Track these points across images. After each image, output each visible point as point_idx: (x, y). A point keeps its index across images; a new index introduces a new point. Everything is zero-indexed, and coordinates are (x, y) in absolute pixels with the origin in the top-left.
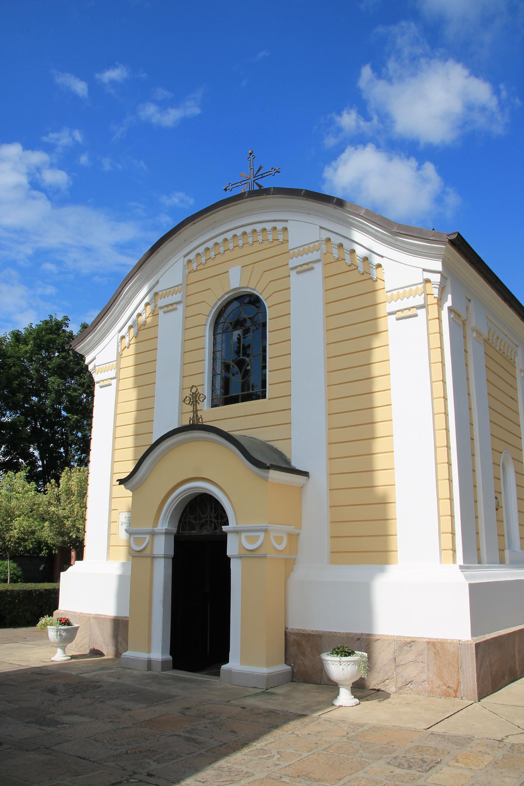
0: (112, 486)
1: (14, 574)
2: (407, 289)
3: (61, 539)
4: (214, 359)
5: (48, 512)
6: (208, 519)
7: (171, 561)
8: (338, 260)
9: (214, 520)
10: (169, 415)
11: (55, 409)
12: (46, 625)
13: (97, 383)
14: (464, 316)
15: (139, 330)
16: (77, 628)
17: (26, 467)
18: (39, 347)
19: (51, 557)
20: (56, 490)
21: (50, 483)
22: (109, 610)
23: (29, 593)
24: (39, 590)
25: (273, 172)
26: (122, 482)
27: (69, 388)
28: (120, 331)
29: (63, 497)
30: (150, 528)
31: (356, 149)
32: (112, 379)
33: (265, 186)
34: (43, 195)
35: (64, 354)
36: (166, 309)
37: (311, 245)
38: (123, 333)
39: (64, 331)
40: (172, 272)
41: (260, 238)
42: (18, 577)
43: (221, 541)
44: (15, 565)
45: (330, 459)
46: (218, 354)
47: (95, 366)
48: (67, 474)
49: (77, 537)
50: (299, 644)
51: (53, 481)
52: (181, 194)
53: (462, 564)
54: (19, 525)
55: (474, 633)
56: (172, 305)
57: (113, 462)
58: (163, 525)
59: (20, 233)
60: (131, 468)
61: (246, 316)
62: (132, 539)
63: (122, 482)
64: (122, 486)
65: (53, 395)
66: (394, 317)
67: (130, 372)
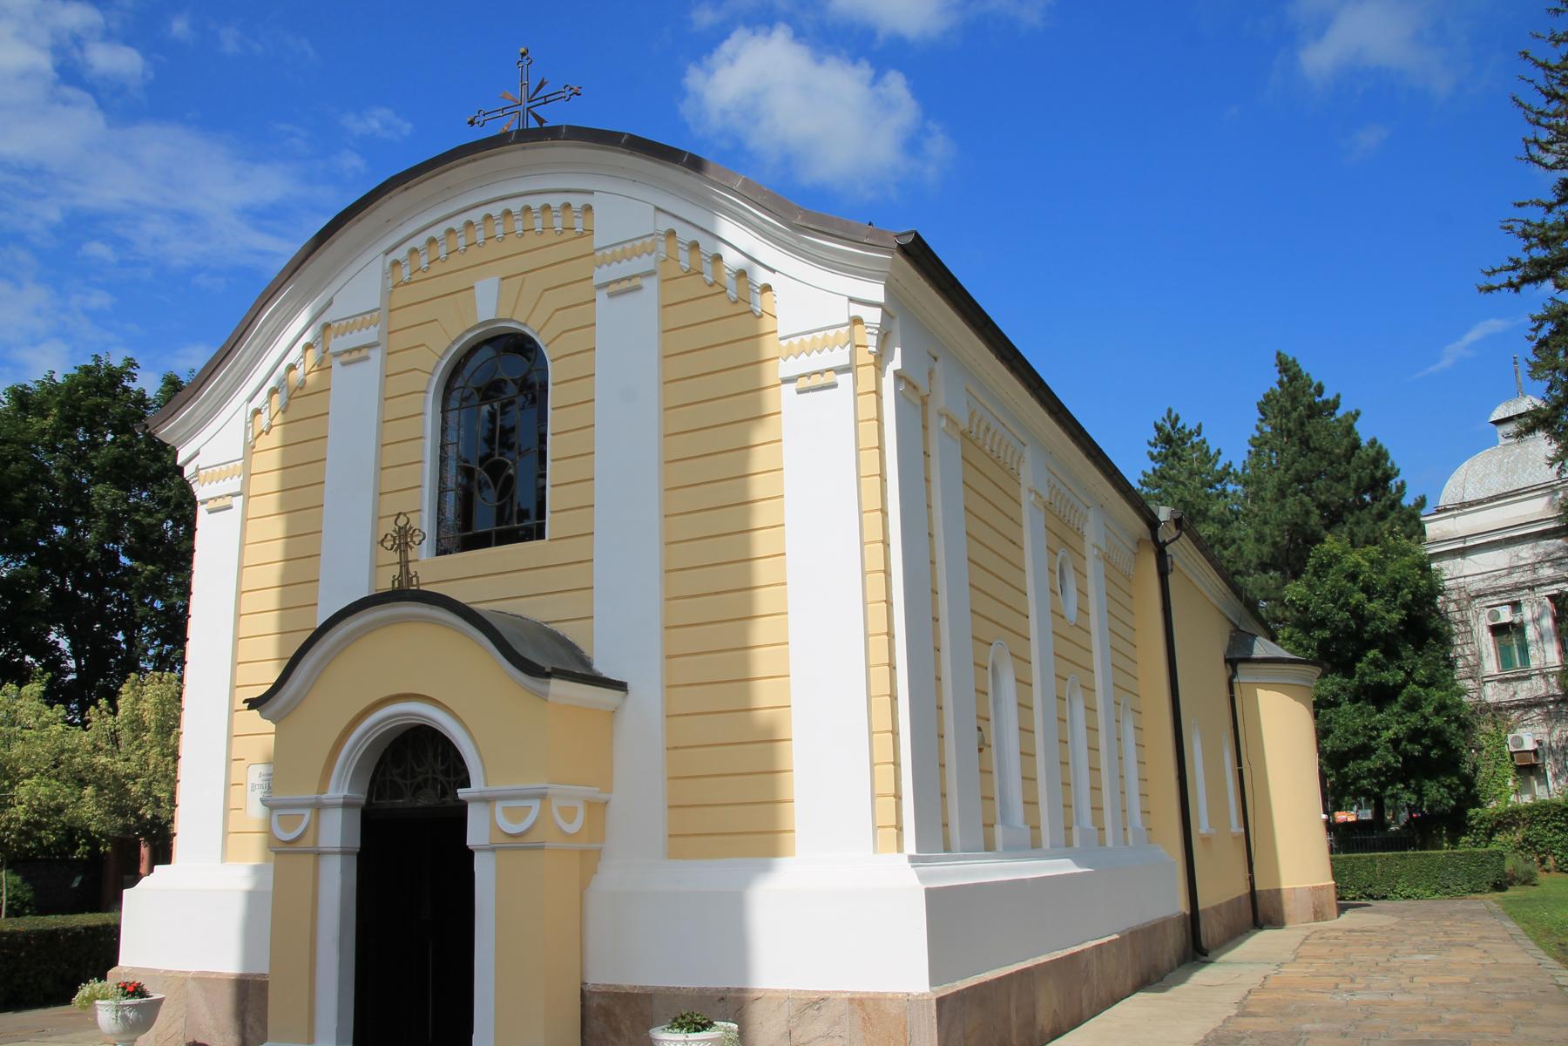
0: (232, 711)
1: (15, 898)
2: (819, 335)
3: (120, 821)
4: (443, 460)
5: (91, 768)
6: (430, 776)
7: (354, 859)
8: (688, 273)
9: (441, 777)
10: (351, 572)
11: (105, 552)
12: (92, 998)
13: (204, 502)
14: (924, 389)
15: (290, 398)
16: (160, 1001)
17: (42, 674)
18: (70, 422)
19: (95, 858)
20: (110, 720)
21: (97, 706)
22: (228, 961)
23: (52, 935)
24: (72, 929)
25: (567, 94)
26: (253, 704)
27: (136, 508)
28: (250, 400)
29: (125, 735)
30: (310, 795)
31: (754, 34)
32: (233, 495)
33: (551, 122)
34: (88, 97)
35: (126, 438)
36: (346, 357)
37: (638, 243)
38: (256, 403)
39: (126, 390)
40: (360, 283)
41: (538, 224)
42: (25, 904)
43: (457, 818)
44: (18, 880)
45: (669, 657)
46: (451, 451)
47: (198, 470)
48: (133, 687)
49: (155, 817)
50: (607, 1013)
51: (103, 702)
52: (386, 113)
53: (913, 852)
54: (29, 794)
55: (934, 980)
56: (358, 349)
57: (236, 663)
58: (339, 789)
59: (35, 177)
60: (271, 674)
61: (505, 376)
62: (275, 819)
63: (253, 704)
64: (255, 712)
65: (102, 523)
66: (792, 387)
67: (272, 482)
